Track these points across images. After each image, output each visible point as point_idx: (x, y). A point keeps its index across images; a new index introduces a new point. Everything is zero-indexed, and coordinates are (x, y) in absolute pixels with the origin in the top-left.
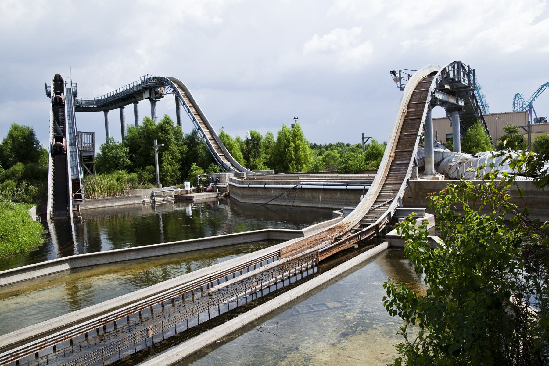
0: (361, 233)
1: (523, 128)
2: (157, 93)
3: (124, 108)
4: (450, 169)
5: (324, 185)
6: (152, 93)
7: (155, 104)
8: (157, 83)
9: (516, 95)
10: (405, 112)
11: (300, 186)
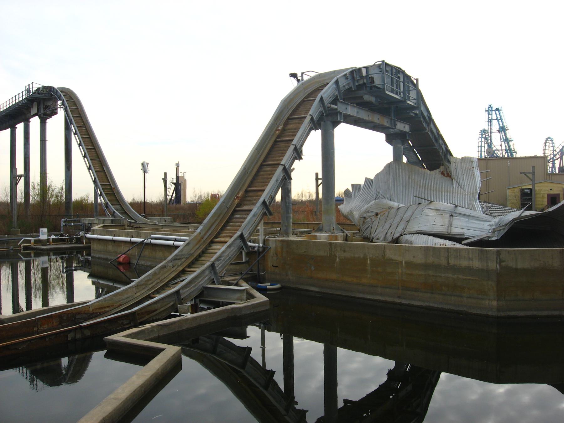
0: (76, 329)
1: (525, 174)
2: (46, 107)
3: (16, 128)
4: (363, 222)
5: (176, 240)
6: (40, 108)
7: (45, 123)
8: (46, 95)
9: (547, 139)
10: (279, 130)
11: (149, 241)
